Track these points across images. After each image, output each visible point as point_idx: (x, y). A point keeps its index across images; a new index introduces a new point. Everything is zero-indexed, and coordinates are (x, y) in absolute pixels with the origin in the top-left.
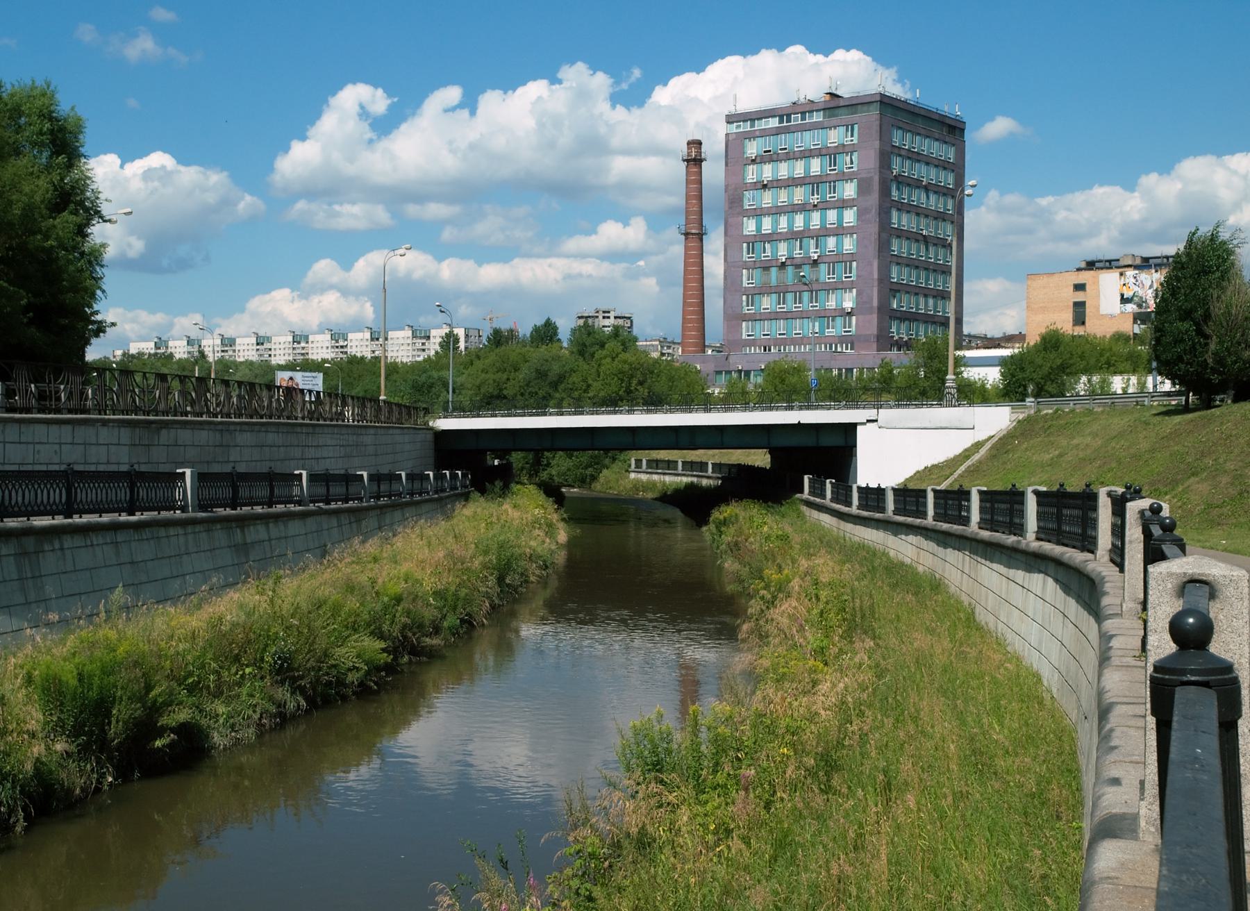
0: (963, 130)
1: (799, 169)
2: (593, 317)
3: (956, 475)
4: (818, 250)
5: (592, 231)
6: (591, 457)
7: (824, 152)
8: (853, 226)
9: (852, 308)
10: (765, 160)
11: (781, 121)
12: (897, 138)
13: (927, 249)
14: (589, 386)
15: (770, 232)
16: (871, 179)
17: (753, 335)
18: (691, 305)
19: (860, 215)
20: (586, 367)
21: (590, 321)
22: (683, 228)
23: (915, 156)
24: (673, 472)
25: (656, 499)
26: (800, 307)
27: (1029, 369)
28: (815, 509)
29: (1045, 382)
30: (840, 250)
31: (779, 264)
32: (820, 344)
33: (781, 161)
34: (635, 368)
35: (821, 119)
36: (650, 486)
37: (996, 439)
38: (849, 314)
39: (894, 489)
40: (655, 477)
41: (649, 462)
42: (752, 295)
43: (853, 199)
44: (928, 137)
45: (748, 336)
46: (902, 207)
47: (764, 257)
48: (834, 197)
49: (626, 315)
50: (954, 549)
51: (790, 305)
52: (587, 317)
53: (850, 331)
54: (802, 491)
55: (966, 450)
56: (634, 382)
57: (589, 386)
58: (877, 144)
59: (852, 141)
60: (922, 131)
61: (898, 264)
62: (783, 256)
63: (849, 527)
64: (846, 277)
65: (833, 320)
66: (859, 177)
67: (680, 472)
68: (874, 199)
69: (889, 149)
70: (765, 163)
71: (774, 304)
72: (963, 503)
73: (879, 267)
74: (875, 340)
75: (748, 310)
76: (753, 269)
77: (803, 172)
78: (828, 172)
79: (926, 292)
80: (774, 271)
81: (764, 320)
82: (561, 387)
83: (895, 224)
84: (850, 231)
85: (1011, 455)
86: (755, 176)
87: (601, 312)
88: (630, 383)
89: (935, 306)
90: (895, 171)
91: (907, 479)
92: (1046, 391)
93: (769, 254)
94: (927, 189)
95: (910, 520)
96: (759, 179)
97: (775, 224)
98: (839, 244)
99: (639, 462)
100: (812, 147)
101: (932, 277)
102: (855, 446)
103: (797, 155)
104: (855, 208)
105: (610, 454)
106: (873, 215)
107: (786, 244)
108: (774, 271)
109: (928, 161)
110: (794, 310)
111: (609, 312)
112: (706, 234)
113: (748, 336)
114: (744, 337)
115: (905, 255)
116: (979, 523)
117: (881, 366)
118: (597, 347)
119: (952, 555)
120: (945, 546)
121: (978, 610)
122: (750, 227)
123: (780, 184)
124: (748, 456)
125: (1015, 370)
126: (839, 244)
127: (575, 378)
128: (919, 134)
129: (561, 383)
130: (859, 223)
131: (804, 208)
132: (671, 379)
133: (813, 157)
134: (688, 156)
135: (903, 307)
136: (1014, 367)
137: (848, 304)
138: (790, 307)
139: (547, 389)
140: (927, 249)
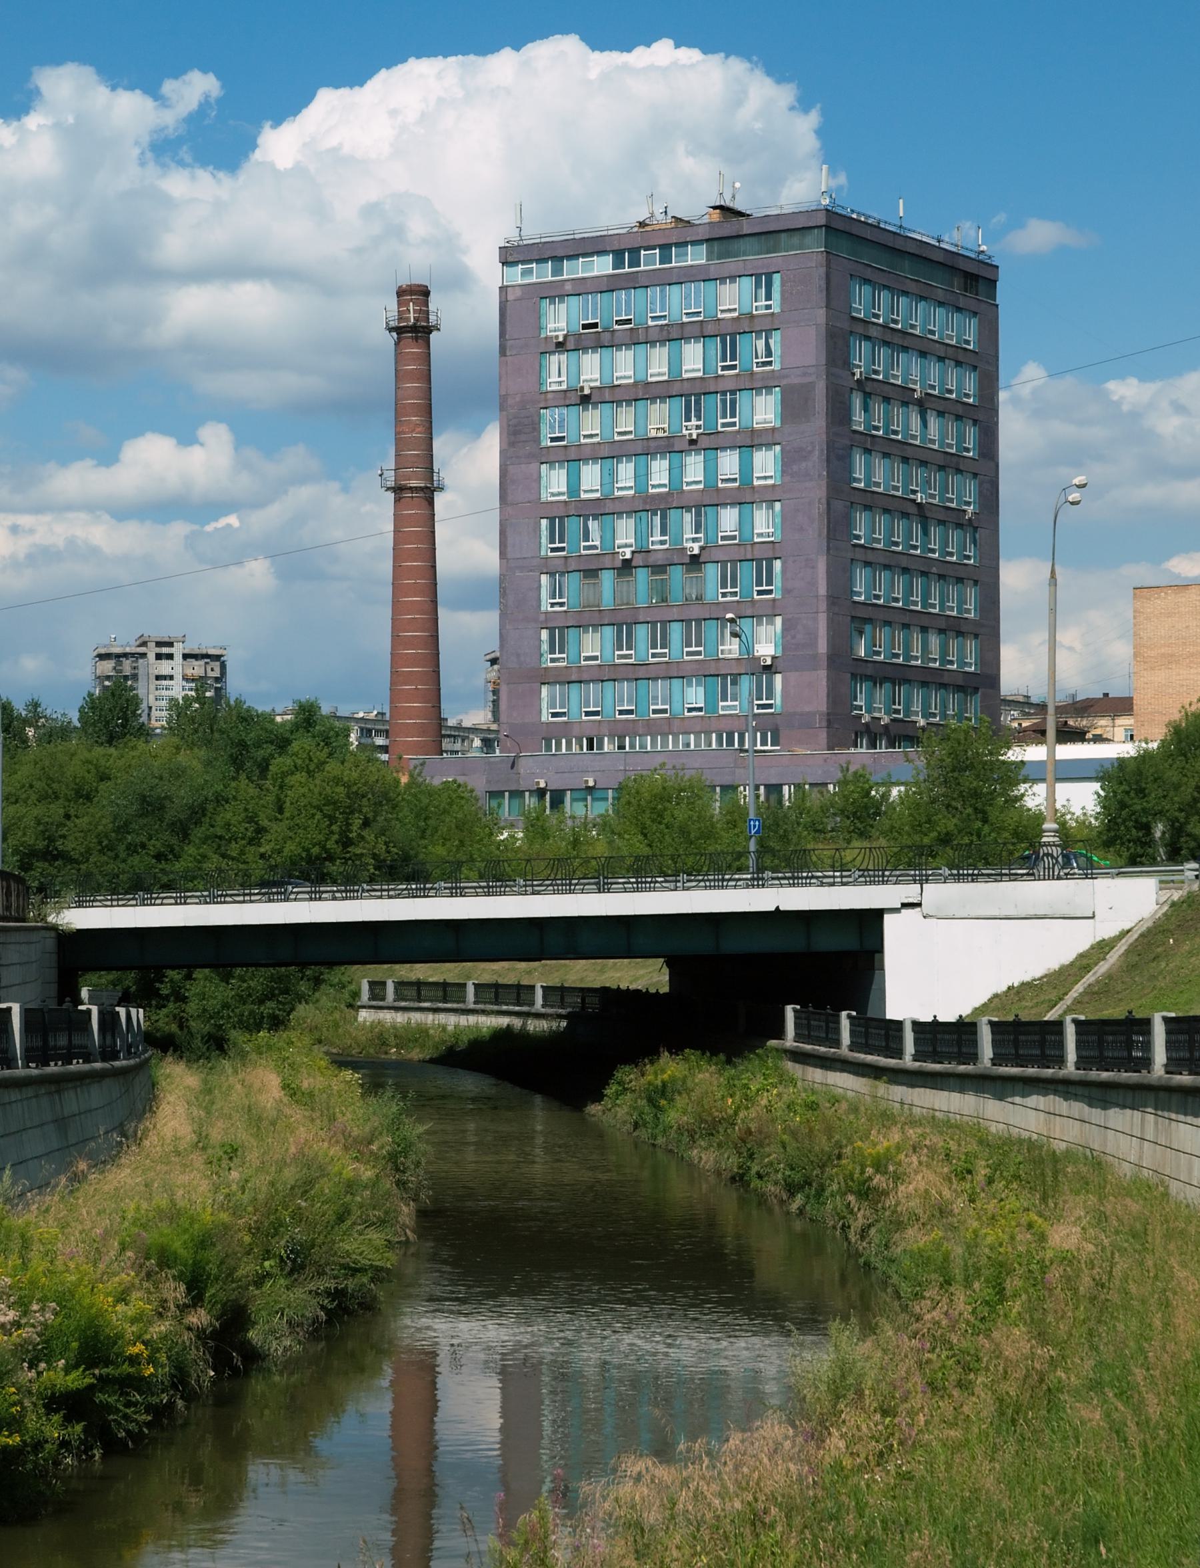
0: (992, 283)
1: (658, 364)
2: (133, 655)
3: (1069, 999)
4: (701, 535)
5: (108, 457)
6: (272, 979)
7: (710, 329)
8: (774, 486)
9: (774, 658)
10: (585, 344)
11: (618, 264)
12: (862, 301)
13: (926, 532)
14: (261, 830)
15: (598, 495)
16: (810, 387)
17: (563, 714)
18: (410, 642)
19: (787, 463)
20: (252, 791)
21: (127, 665)
22: (390, 476)
23: (897, 340)
24: (455, 1006)
25: (432, 1061)
26: (664, 655)
27: (1154, 793)
28: (816, 1066)
29: (1187, 818)
30: (747, 535)
31: (619, 564)
32: (708, 734)
33: (619, 346)
34: (356, 793)
35: (704, 261)
36: (408, 1037)
37: (1134, 936)
38: (767, 668)
39: (916, 1025)
40: (416, 1017)
41: (400, 985)
42: (561, 629)
43: (773, 429)
44: (922, 298)
45: (554, 715)
46: (870, 444)
47: (586, 548)
48: (734, 424)
49: (212, 652)
50: (1124, 1107)
51: (642, 649)
52: (118, 656)
53: (770, 706)
54: (780, 1033)
55: (1081, 956)
56: (357, 822)
57: (261, 830)
58: (821, 315)
59: (768, 307)
60: (912, 287)
61: (867, 564)
62: (626, 546)
63: (899, 1092)
64: (760, 593)
65: (734, 683)
66: (784, 382)
67: (472, 1006)
68: (816, 426)
69: (846, 325)
70: (585, 350)
71: (609, 646)
72: (1135, 1038)
73: (828, 572)
74: (824, 724)
75: (553, 660)
76: (562, 574)
77: (666, 370)
78: (720, 372)
79: (925, 622)
80: (607, 578)
81: (587, 682)
82: (198, 833)
83: (859, 481)
84: (768, 497)
85: (1163, 965)
86: (564, 378)
87: (152, 645)
88: (348, 824)
89: (944, 651)
90: (857, 371)
91: (976, 1009)
92: (1189, 835)
93: (597, 543)
94: (923, 405)
95: (1031, 1071)
96: (573, 384)
97: (607, 479)
98: (745, 523)
99: (377, 988)
100: (685, 319)
101: (935, 589)
102: (880, 949)
103: (653, 335)
104: (778, 448)
105: (308, 972)
106: (816, 463)
107: (632, 522)
108: (607, 578)
109: (925, 349)
110: (652, 660)
111: (170, 644)
112: (441, 489)
113: (554, 715)
114: (545, 717)
115: (880, 546)
116: (1166, 1066)
117: (842, 783)
118: (270, 748)
119: (1119, 1118)
120: (1105, 1105)
121: (1174, 1187)
122: (555, 483)
123: (619, 395)
124: (602, 971)
125: (1127, 793)
126: (745, 523)
127: (230, 815)
128: (905, 293)
129: (198, 823)
130: (787, 479)
131: (668, 446)
132: (422, 814)
133: (687, 339)
134: (400, 319)
135: (878, 654)
136: (1125, 787)
137: (766, 650)
138: (642, 654)
139: (166, 836)
140: (926, 532)
